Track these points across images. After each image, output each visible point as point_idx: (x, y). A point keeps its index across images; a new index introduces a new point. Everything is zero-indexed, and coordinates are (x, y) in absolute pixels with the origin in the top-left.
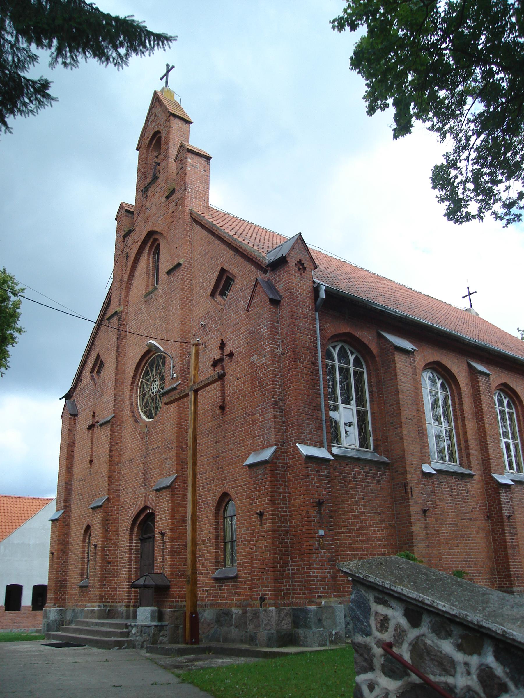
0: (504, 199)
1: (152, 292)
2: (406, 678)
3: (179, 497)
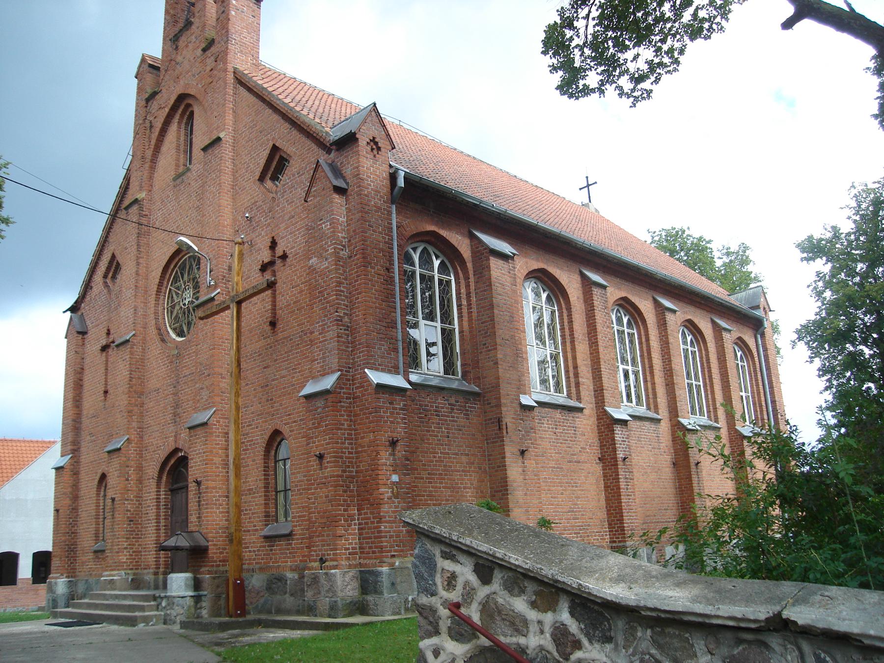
0: (632, 70)
1: (183, 174)
2: (474, 641)
3: (218, 436)
